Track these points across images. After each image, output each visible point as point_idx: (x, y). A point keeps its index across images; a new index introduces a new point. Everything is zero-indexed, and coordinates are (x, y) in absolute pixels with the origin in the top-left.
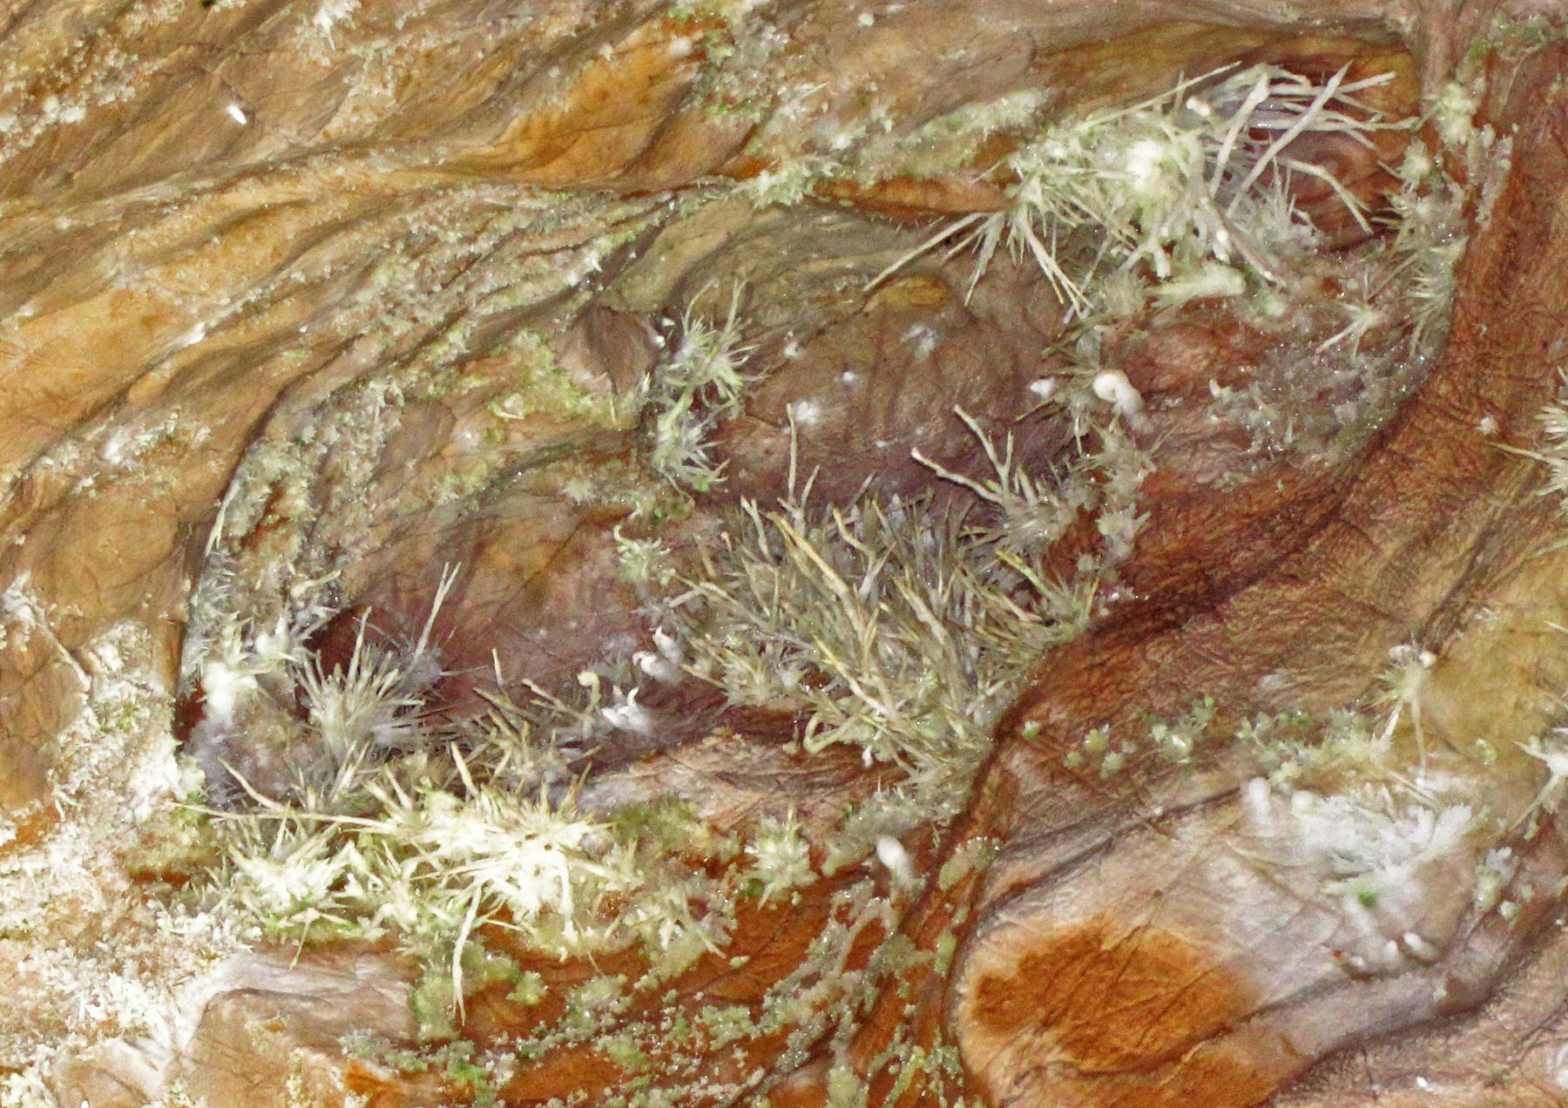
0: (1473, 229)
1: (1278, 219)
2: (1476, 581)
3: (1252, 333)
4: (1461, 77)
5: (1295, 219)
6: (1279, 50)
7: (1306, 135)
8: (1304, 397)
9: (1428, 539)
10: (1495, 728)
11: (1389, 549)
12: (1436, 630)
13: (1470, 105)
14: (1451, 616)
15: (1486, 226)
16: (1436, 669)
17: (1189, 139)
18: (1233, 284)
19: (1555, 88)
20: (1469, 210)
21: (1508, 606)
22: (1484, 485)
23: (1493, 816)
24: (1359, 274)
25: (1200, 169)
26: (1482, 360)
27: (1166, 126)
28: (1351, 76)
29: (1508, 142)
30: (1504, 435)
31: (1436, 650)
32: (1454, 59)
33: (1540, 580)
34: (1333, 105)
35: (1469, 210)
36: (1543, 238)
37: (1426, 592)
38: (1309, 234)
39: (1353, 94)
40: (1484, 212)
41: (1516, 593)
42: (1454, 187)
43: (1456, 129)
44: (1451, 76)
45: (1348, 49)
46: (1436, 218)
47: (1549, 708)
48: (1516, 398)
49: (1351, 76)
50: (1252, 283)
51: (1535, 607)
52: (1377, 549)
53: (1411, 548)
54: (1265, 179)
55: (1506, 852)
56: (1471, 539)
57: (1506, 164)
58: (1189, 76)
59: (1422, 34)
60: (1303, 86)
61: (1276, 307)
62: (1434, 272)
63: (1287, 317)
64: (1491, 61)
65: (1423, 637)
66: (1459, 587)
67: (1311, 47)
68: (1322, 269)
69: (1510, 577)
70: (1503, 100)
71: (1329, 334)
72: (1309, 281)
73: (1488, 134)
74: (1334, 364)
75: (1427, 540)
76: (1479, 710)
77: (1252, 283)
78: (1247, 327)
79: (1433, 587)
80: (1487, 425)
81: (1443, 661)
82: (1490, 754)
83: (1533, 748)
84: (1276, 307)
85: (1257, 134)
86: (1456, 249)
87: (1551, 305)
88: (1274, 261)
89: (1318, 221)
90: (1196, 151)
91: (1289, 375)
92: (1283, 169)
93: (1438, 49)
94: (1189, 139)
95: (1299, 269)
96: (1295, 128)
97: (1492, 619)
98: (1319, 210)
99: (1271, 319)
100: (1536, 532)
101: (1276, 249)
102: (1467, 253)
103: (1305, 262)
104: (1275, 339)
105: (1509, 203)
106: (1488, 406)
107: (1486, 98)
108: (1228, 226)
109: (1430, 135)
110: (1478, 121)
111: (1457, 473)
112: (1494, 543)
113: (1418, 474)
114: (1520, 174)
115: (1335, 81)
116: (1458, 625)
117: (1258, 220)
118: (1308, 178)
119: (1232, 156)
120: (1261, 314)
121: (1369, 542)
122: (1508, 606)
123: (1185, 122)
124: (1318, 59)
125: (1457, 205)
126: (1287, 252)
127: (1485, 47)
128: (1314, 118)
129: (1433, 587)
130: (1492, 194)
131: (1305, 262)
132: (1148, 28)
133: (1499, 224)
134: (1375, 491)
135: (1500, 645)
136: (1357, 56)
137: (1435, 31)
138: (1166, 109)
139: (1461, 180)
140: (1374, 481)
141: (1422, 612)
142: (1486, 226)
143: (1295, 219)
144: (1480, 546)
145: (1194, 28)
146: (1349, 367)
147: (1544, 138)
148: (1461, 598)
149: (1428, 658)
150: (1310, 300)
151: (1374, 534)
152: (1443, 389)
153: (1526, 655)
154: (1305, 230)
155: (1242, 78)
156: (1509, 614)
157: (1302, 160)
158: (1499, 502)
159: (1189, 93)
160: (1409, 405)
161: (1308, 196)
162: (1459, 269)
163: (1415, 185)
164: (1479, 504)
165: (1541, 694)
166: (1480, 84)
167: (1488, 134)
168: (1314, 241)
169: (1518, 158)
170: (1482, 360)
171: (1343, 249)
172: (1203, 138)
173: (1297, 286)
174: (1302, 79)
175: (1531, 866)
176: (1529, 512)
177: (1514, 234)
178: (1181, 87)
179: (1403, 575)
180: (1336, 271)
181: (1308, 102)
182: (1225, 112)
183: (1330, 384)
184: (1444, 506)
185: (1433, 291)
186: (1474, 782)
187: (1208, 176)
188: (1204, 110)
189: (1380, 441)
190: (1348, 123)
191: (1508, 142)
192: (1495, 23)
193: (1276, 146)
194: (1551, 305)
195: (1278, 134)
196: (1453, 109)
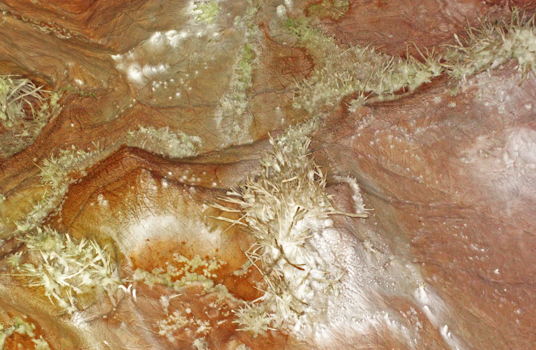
0: (48, 122)
1: (18, 109)
2: (20, 188)
3: (4, 128)
4: (58, 93)
5: (22, 111)
6: (32, 78)
7: (29, 96)
8: (7, 143)
9: (15, 176)
10: (11, 216)
11: (7, 175)
12: (8, 194)
13: (58, 99)
14: (12, 192)
15: (51, 122)
16: (5, 201)
17: (7, 87)
18: (4, 117)
19: (74, 101)
20: (49, 118)
21: (23, 194)
22: (29, 170)
23: (4, 233)
24: (27, 125)
25: (7, 93)
26: (39, 147)
27: (4, 82)
28: (44, 88)
29: (61, 108)
30: (37, 163)
31: (7, 197)
32: (59, 89)
33: (31, 191)
34: (38, 92)
35: (49, 118)
36: (59, 128)
37: (10, 186)
38: (23, 115)
39: (43, 92)
40: (52, 119)
41: (26, 193)
42: (49, 113)
43: (53, 102)
44: (57, 92)
45: (45, 83)
46: (43, 117)
47: (23, 217)
48: (42, 156)
49: (44, 88)
50: (8, 118)
51: (28, 197)
52: (4, 175)
53: (11, 177)
54: (19, 101)
55: (3, 241)
56: (22, 179)
57: (59, 112)
58: (11, 74)
59: (56, 83)
60: (34, 86)
61: (10, 125)
62: (39, 128)
63: (11, 128)
64: (65, 92)
65: (6, 195)
66: (16, 187)
67: (38, 80)
68: (22, 122)
69: (26, 189)
70: (64, 100)
71: (18, 134)
72: (19, 123)
73: (59, 105)
74: (16, 139)
75: (14, 176)
76: (10, 212)
77: (8, 118)
78: (3, 127)
79: (11, 186)
80: (35, 159)
81: (7, 200)
82: (8, 221)
83: (16, 224)
84: (10, 125)
85: (22, 92)
86: (44, 125)
87: (55, 141)
88: (14, 117)
89: (26, 113)
90: (8, 89)
91: (6, 138)
92: (23, 100)
93: (57, 87)
94: (7, 87)
95: (18, 119)
96: (28, 93)
97: (19, 196)
98: (27, 111)
99: (8, 127)
100: (34, 183)
101: (15, 115)
102: (45, 126)
103: (19, 119)
104: (7, 131)
105: (57, 120)
106: (37, 156)
107: (61, 99)
108: (7, 105)
109: (49, 101)
110: (58, 102)
111: (25, 166)
112: (26, 181)
113: (19, 163)
114: (61, 115)
115: (39, 88)
116: (13, 195)
117: (14, 108)
118: (28, 104)
119: (14, 93)
120: (7, 125)
121: (4, 172)
122: (23, 194)
123: (8, 83)
124: (39, 83)
125: (48, 117)
126: (17, 116)
127: (65, 89)
128: (33, 93)
129: (11, 186)
130: (55, 117)
131: (19, 119)
132: (6, 61)
133: (53, 123)
134: (9, 164)
135: (18, 201)
136: (46, 85)
137: (58, 83)
138: (5, 79)
139: (50, 112)
140: (10, 162)
141: (7, 190)
142: (51, 122)
143: (22, 111)
144: (23, 181)
145: (15, 65)
146: (18, 141)
147: (68, 109)
148: (16, 189)
149: (4, 198)
150: (17, 127)
151: (5, 171)
152: (30, 150)
153: (23, 205)
154: (22, 113)
155: (22, 80)
156: (22, 196)
157: (29, 101)
158: (30, 175)
159: (11, 77)
160: (23, 151)
161: (26, 108)
162: (43, 129)
163: (43, 110)
164: (26, 173)
165: (22, 214)
166: (61, 95)
167: (59, 105)
168: (23, 116)
169: (62, 112)
170: (39, 147)
171: (27, 120)
172: (10, 88)
173: (16, 123)
174: (34, 85)
175: (6, 245)
176: (35, 178)
177: (55, 126)
178: (9, 76)
179: (7, 181)
180: (25, 123)
181: (33, 89)
182: (16, 85)
183: (13, 143)
184: (21, 171)
185: (37, 132)
186: (3, 225)
187: (8, 95)
188: (11, 82)
189: (15, 155)
190: (40, 97)
191: (61, 108)
192: (69, 85)
193: (23, 95)
194: (55, 141)
195: (25, 93)
196: (55, 98)
